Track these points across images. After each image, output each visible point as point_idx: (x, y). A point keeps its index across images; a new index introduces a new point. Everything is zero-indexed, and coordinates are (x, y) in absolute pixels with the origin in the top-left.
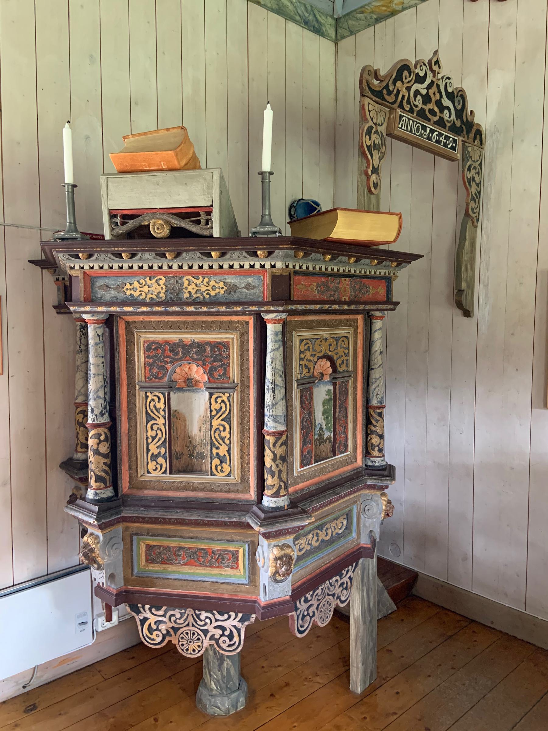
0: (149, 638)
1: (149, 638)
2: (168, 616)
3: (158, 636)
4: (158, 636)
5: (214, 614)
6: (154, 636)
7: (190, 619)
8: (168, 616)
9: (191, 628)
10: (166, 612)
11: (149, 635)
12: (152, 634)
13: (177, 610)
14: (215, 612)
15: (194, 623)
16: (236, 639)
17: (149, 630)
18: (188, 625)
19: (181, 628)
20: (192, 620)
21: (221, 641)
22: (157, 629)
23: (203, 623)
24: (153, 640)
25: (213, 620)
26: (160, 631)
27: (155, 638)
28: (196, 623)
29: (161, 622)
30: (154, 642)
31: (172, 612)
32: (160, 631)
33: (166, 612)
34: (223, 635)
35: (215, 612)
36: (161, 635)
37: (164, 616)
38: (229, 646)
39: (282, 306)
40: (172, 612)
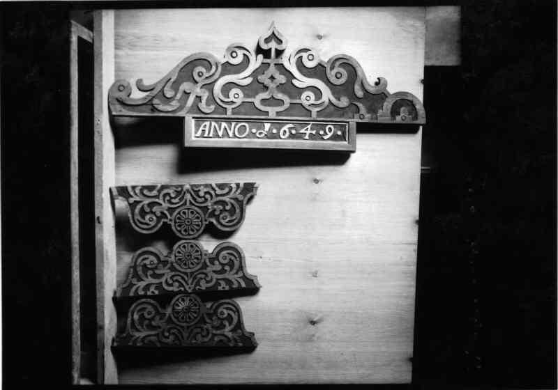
0: (231, 309)
1: (231, 309)
2: (210, 335)
3: (225, 258)
4: (222, 313)
5: (160, 342)
6: (229, 257)
7: (185, 335)
8: (210, 335)
9: (184, 324)
10: (212, 339)
11: (233, 258)
12: (230, 259)
13: (204, 288)
14: (159, 345)
15: (182, 330)
16: (136, 317)
17: (232, 318)
18: (188, 327)
19: (199, 269)
20: (184, 334)
21: (156, 261)
22: (223, 265)
23: (172, 331)
24: (227, 309)
25: (160, 335)
26: (220, 264)
27: (235, 100)
28: (179, 330)
29: (217, 328)
30: (225, 306)
31: (206, 340)
32: (220, 264)
33: (212, 339)
34: (150, 320)
35: (159, 345)
36: (220, 259)
37: (215, 335)
38: (144, 309)
39: (139, 320)
40: (206, 340)
